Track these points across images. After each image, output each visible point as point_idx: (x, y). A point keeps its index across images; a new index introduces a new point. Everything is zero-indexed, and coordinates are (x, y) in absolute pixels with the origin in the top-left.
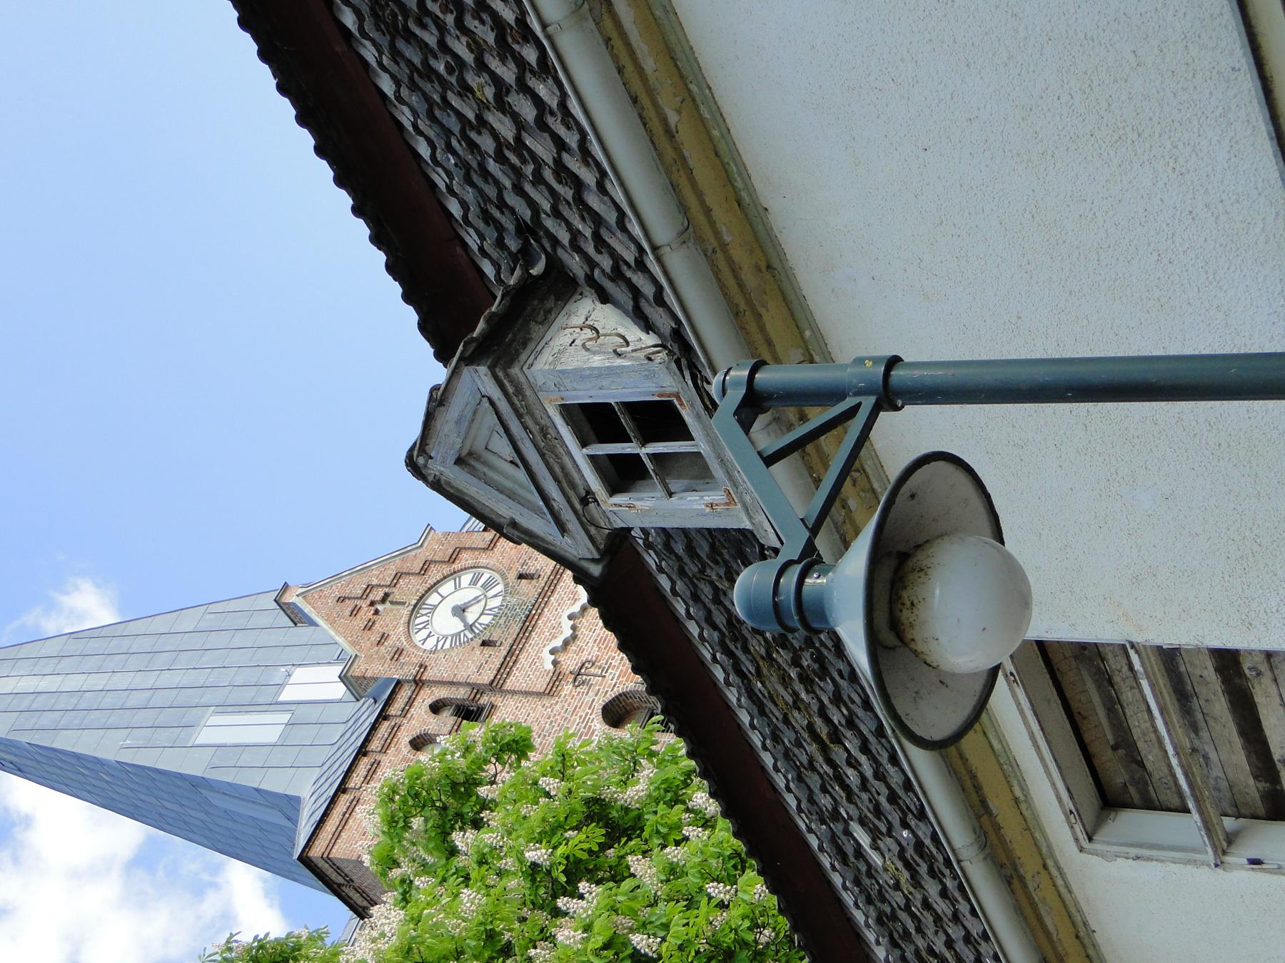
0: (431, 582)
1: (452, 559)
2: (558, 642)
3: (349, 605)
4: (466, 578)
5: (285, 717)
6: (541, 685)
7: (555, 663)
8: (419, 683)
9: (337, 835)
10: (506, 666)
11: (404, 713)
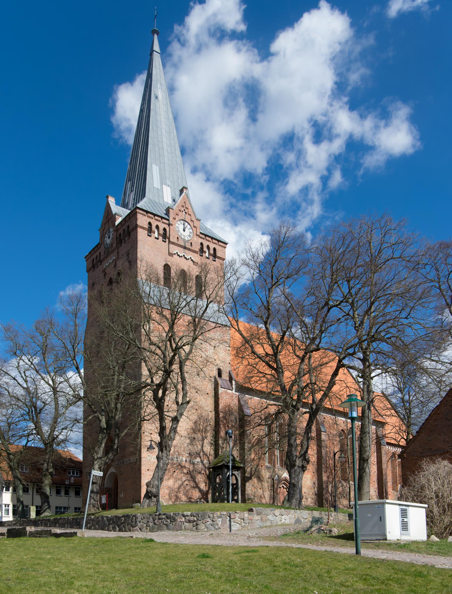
0: (190, 223)
1: (194, 227)
2: (179, 254)
3: (184, 204)
4: (191, 231)
5: (159, 188)
6: (171, 251)
7: (175, 254)
8: (169, 225)
9: (142, 214)
10: (173, 243)
11: (163, 222)
